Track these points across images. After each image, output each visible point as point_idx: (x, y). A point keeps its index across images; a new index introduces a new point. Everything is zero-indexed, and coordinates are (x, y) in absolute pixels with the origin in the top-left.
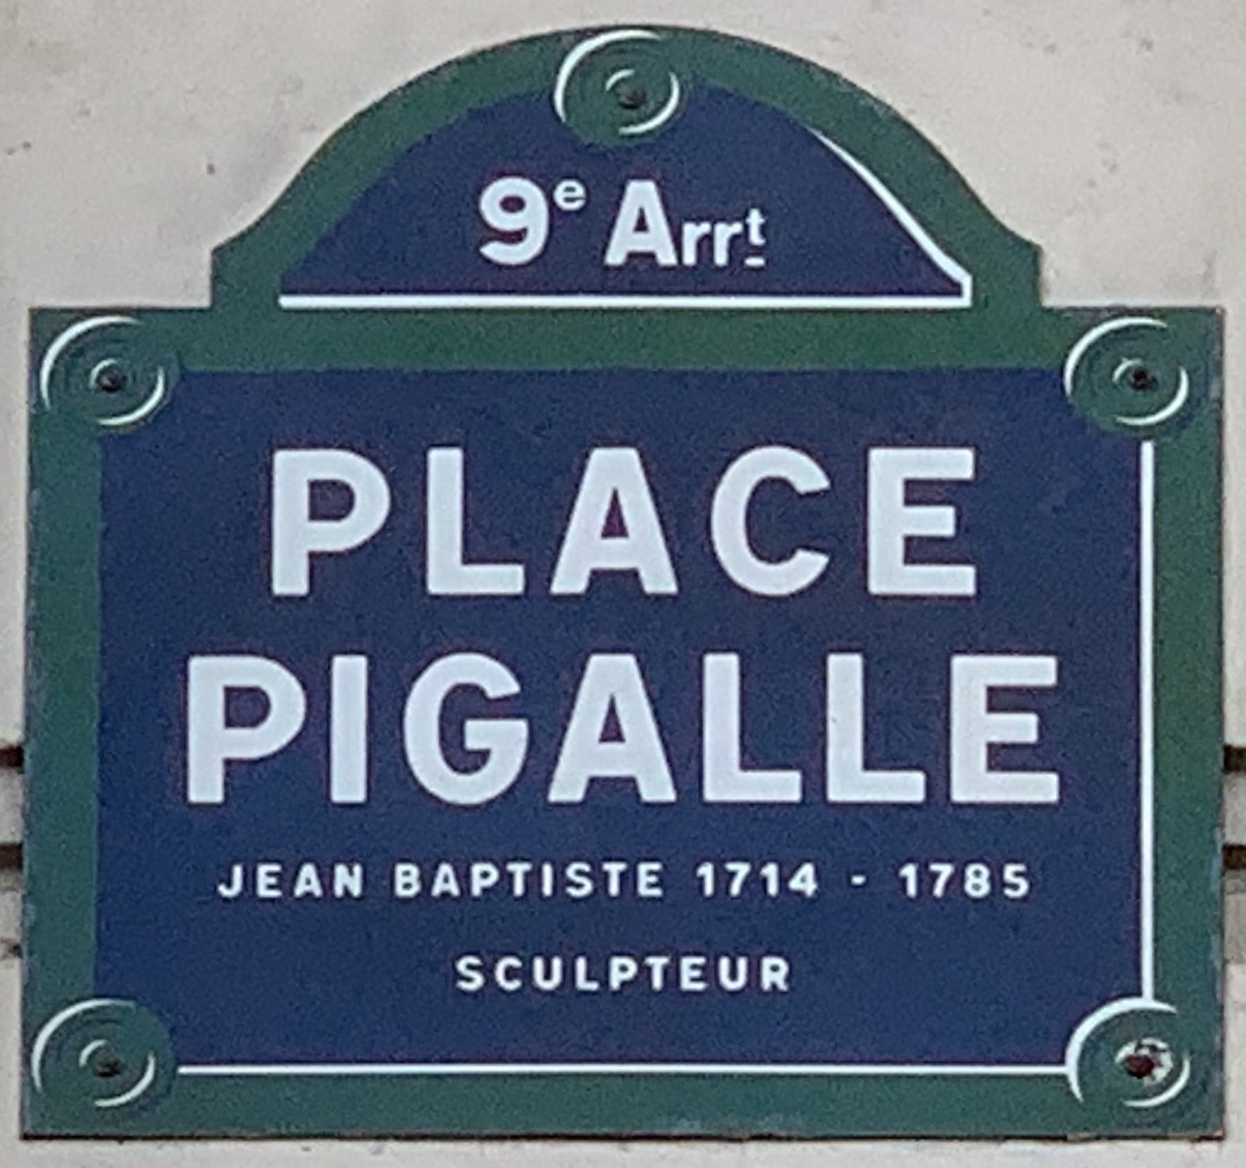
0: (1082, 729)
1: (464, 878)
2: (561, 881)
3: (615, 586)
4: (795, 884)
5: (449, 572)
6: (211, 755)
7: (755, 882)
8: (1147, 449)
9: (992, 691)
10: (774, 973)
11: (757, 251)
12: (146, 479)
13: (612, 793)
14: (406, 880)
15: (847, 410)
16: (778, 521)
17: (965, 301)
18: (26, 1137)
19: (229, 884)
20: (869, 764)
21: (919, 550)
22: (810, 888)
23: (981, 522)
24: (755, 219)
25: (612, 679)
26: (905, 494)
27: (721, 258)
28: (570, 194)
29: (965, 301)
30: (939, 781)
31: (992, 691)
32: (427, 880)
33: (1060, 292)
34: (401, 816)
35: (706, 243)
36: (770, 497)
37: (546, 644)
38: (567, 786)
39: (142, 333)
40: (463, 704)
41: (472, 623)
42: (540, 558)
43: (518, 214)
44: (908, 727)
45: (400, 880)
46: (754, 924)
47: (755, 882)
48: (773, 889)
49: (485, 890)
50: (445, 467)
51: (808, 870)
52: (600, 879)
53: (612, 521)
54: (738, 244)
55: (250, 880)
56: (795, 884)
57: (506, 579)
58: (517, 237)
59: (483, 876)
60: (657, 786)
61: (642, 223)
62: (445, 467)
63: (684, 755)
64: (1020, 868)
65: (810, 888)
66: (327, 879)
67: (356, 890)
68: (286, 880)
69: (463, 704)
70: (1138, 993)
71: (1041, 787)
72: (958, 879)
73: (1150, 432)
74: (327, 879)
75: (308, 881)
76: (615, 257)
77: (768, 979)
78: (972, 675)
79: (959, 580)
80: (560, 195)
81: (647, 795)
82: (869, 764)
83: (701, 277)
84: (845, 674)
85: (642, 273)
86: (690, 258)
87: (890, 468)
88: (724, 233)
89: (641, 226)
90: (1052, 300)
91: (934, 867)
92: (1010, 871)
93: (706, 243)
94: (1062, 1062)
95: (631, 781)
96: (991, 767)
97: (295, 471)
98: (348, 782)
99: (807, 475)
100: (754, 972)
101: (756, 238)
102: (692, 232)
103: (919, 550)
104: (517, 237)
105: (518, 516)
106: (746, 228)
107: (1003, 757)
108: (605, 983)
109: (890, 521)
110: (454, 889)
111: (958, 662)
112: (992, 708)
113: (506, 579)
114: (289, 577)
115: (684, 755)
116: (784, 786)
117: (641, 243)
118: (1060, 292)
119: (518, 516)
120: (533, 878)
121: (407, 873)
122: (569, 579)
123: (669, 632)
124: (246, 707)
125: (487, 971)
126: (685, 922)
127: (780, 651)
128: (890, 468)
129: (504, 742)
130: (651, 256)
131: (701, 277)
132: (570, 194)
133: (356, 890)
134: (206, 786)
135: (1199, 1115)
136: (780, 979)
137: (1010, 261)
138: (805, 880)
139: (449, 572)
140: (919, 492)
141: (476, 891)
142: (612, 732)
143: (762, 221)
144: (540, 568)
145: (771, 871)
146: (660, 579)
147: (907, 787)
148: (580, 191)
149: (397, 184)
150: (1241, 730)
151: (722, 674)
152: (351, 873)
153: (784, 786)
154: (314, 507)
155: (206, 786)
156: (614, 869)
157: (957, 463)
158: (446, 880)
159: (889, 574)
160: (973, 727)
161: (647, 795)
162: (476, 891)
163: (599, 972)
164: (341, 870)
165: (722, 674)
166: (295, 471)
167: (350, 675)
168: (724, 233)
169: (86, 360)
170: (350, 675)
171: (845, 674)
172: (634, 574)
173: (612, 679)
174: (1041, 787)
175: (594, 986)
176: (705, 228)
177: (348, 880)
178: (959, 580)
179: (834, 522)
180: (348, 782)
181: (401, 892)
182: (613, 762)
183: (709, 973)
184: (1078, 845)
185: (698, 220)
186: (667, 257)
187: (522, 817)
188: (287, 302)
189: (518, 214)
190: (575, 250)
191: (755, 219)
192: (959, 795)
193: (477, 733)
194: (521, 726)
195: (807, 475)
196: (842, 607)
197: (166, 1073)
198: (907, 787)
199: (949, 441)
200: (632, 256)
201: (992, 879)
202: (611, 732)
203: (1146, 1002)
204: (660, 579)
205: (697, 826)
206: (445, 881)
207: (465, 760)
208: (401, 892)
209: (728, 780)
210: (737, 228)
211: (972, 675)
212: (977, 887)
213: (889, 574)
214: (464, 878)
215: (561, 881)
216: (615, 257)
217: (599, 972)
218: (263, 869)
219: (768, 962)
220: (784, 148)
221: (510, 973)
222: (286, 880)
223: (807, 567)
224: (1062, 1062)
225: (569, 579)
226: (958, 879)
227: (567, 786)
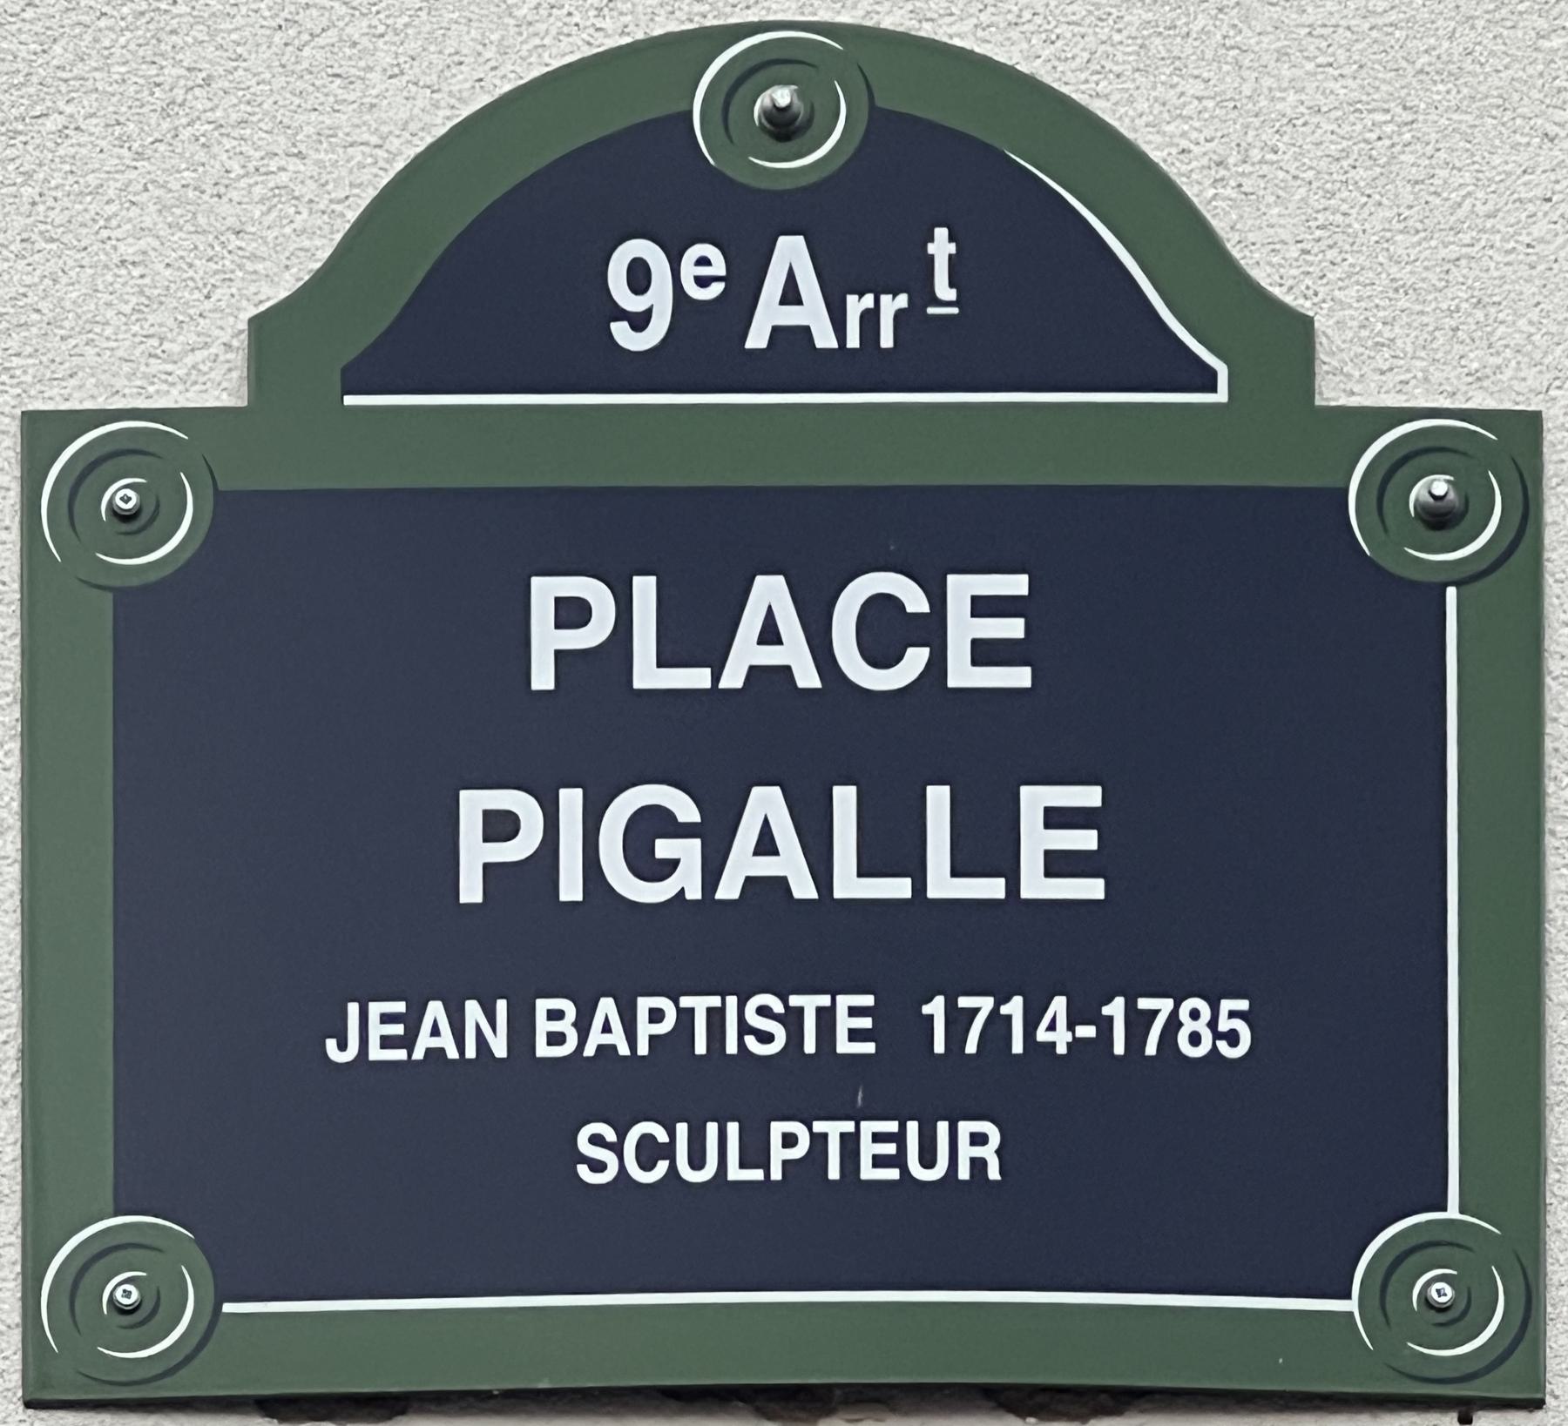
7: (998, 1025)
8: (1451, 592)
17: (1221, 396)
29: (1221, 396)
33: (1342, 383)
35: (870, 319)
39: (150, 445)
40: (651, 823)
43: (651, 286)
47: (998, 1025)
56: (1042, 1035)
58: (640, 322)
61: (793, 294)
63: (822, 870)
73: (1465, 577)
85: (793, 358)
86: (853, 341)
87: (962, 588)
88: (892, 304)
90: (1331, 392)
93: (870, 319)
98: (571, 888)
102: (855, 306)
109: (963, 629)
115: (822, 870)
118: (1342, 383)
143: (952, 248)
148: (719, 267)
149: (498, 245)
160: (1035, 840)
167: (571, 800)
170: (571, 800)
176: (868, 301)
180: (571, 888)
186: (825, 338)
188: (349, 400)
189: (651, 286)
193: (664, 848)
194: (697, 842)
207: (650, 869)
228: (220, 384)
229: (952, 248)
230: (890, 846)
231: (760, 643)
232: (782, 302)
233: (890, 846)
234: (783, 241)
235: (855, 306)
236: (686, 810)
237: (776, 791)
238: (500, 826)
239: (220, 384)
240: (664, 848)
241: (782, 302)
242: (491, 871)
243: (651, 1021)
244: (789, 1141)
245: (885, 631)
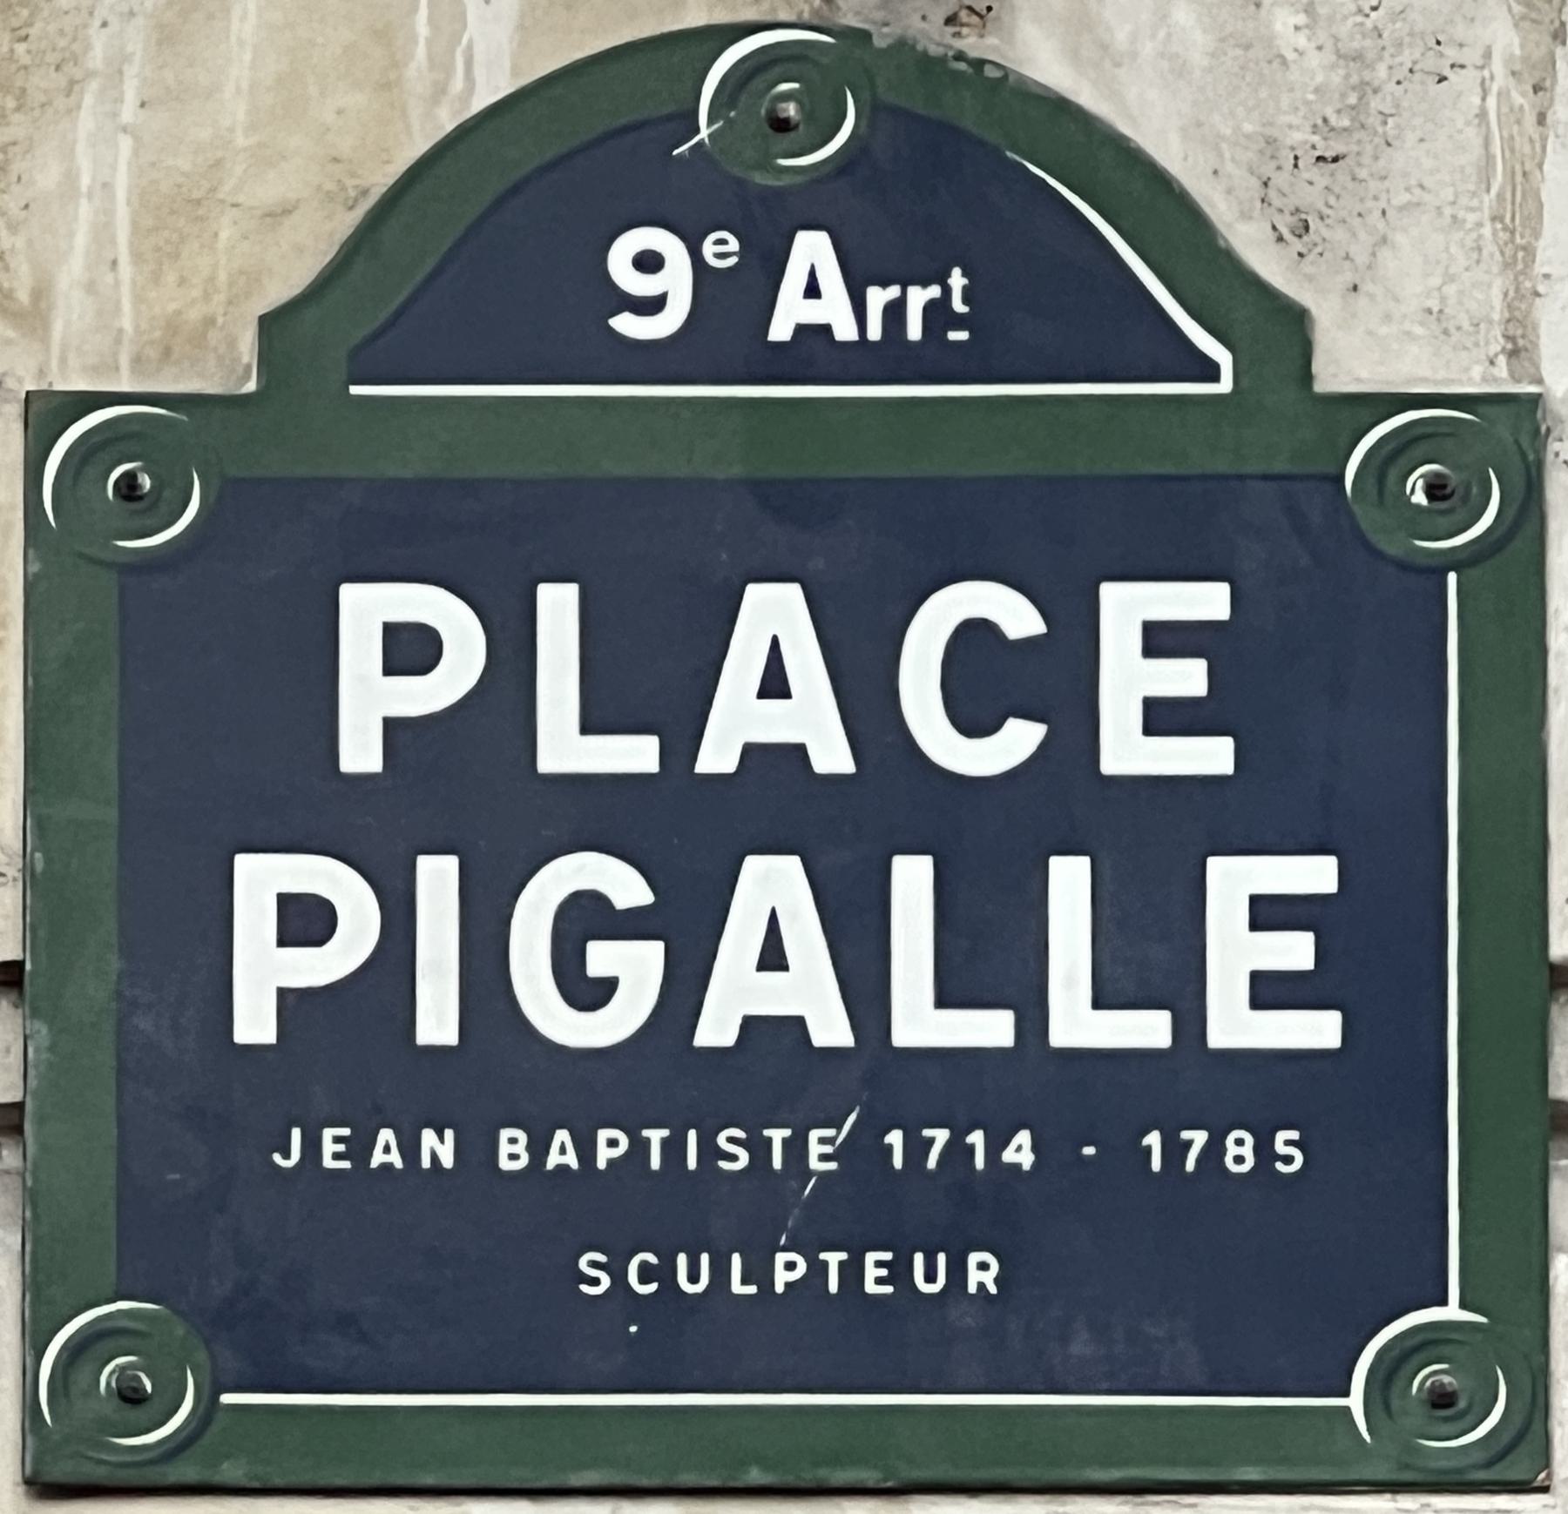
1: (586, 1149)
2: (710, 1152)
3: (776, 763)
4: (1009, 1156)
5: (564, 746)
6: (263, 979)
7: (958, 1151)
8: (1452, 578)
9: (1257, 978)
10: (982, 1272)
11: (959, 322)
12: (183, 594)
13: (773, 1036)
14: (512, 1150)
16: (982, 679)
17: (1225, 385)
19: (286, 1155)
21: (1162, 717)
22: (1026, 1159)
23: (1242, 681)
24: (957, 280)
25: (772, 887)
26: (1143, 641)
27: (914, 331)
29: (1225, 385)
31: (1257, 978)
32: (539, 1148)
33: (1342, 366)
34: (502, 1065)
35: (895, 312)
37: (689, 839)
38: (716, 1028)
39: (170, 433)
40: (584, 918)
42: (682, 731)
44: (1152, 953)
45: (504, 1149)
47: (958, 1151)
48: (980, 1162)
49: (611, 1162)
50: (558, 608)
51: (1024, 1138)
52: (759, 1148)
53: (774, 685)
54: (937, 313)
55: (312, 1146)
56: (1009, 1156)
57: (638, 754)
58: (653, 306)
59: (610, 1146)
60: (831, 1028)
61: (814, 289)
62: (558, 608)
63: (865, 986)
64: (1294, 1135)
65: (1026, 1159)
66: (410, 1149)
67: (447, 1161)
68: (358, 1148)
69: (584, 918)
70: (1443, 1301)
71: (1319, 1030)
72: (1215, 1149)
73: (1461, 561)
74: (410, 1149)
76: (780, 330)
77: (974, 1278)
78: (1232, 881)
79: (1212, 756)
80: (708, 249)
81: (820, 1039)
83: (886, 357)
84: (1070, 881)
86: (875, 332)
87: (1125, 607)
88: (918, 298)
89: (812, 291)
91: (1186, 1135)
92: (1283, 1140)
93: (895, 312)
94: (1346, 1394)
95: (800, 1022)
96: (1255, 926)
98: (437, 1020)
99: (1018, 617)
100: (958, 1271)
101: (959, 306)
102: (877, 298)
104: (653, 306)
105: (650, 676)
106: (947, 291)
108: (766, 1282)
109: (1127, 678)
110: (571, 1160)
111: (1215, 865)
112: (1257, 1003)
113: (638, 754)
114: (360, 752)
115: (865, 986)
116: (992, 1029)
117: (813, 313)
118: (1342, 366)
119: (650, 676)
120: (674, 1148)
121: (513, 1141)
122: (717, 755)
123: (846, 825)
124: (305, 921)
125: (618, 1274)
126: (867, 1205)
127: (990, 851)
128: (1125, 607)
129: (635, 968)
130: (826, 329)
132: (721, 249)
133: (447, 1161)
134: (255, 1022)
135: (1520, 1459)
136: (988, 1278)
138: (1020, 1152)
139: (564, 746)
140: (1161, 640)
141: (601, 1164)
142: (773, 957)
143: (965, 281)
144: (682, 738)
145: (977, 1138)
146: (832, 755)
147: (1149, 1029)
148: (734, 245)
150: (1566, 944)
151: (912, 880)
152: (434, 1157)
153: (992, 1029)
154: (391, 660)
155: (255, 1022)
156: (778, 1136)
157: (1209, 601)
158: (563, 1151)
159: (1126, 750)
160: (1234, 951)
161: (820, 1039)
162: (601, 1164)
163: (759, 1272)
164: (428, 1137)
165: (912, 880)
167: (437, 879)
168: (918, 298)
169: (103, 456)
170: (437, 879)
171: (1070, 881)
172: (800, 751)
173: (772, 887)
174: (1319, 1030)
175: (752, 1289)
176: (894, 292)
177: (439, 1147)
178: (1212, 756)
179: (1054, 677)
180: (437, 1020)
181: (505, 1164)
182: (774, 997)
183: (898, 1273)
184: (1367, 1102)
185: (884, 284)
186: (845, 330)
188: (355, 390)
189: (657, 275)
190: (730, 317)
191: (957, 280)
192: (1218, 1038)
193: (601, 957)
195: (1018, 617)
196: (1066, 796)
198: (1149, 1029)
200: (801, 330)
201: (1257, 1150)
202: (772, 960)
203: (1451, 1312)
204: (832, 755)
205: (882, 1076)
206: (562, 1153)
207: (590, 994)
208: (505, 1164)
209: (920, 1021)
210: (934, 291)
211: (1232, 881)
212: (1239, 1160)
213: (1126, 750)
214: (586, 1149)
215: (710, 1152)
217: (759, 1272)
218: (328, 1134)
219: (974, 1258)
220: (991, 191)
221: (646, 1274)
222: (358, 1148)
223: (1018, 740)
224: (1346, 1394)
225: (717, 755)
226: (1215, 1149)
227: (716, 1028)
229: (965, 281)
230: (990, 953)
231: (785, 968)
232: (762, 694)
233: (990, 953)
234: (754, 865)
235: (877, 298)
236: (626, 887)
237: (791, 865)
238: (305, 921)
240: (601, 957)
241: (762, 694)
242: (290, 1001)
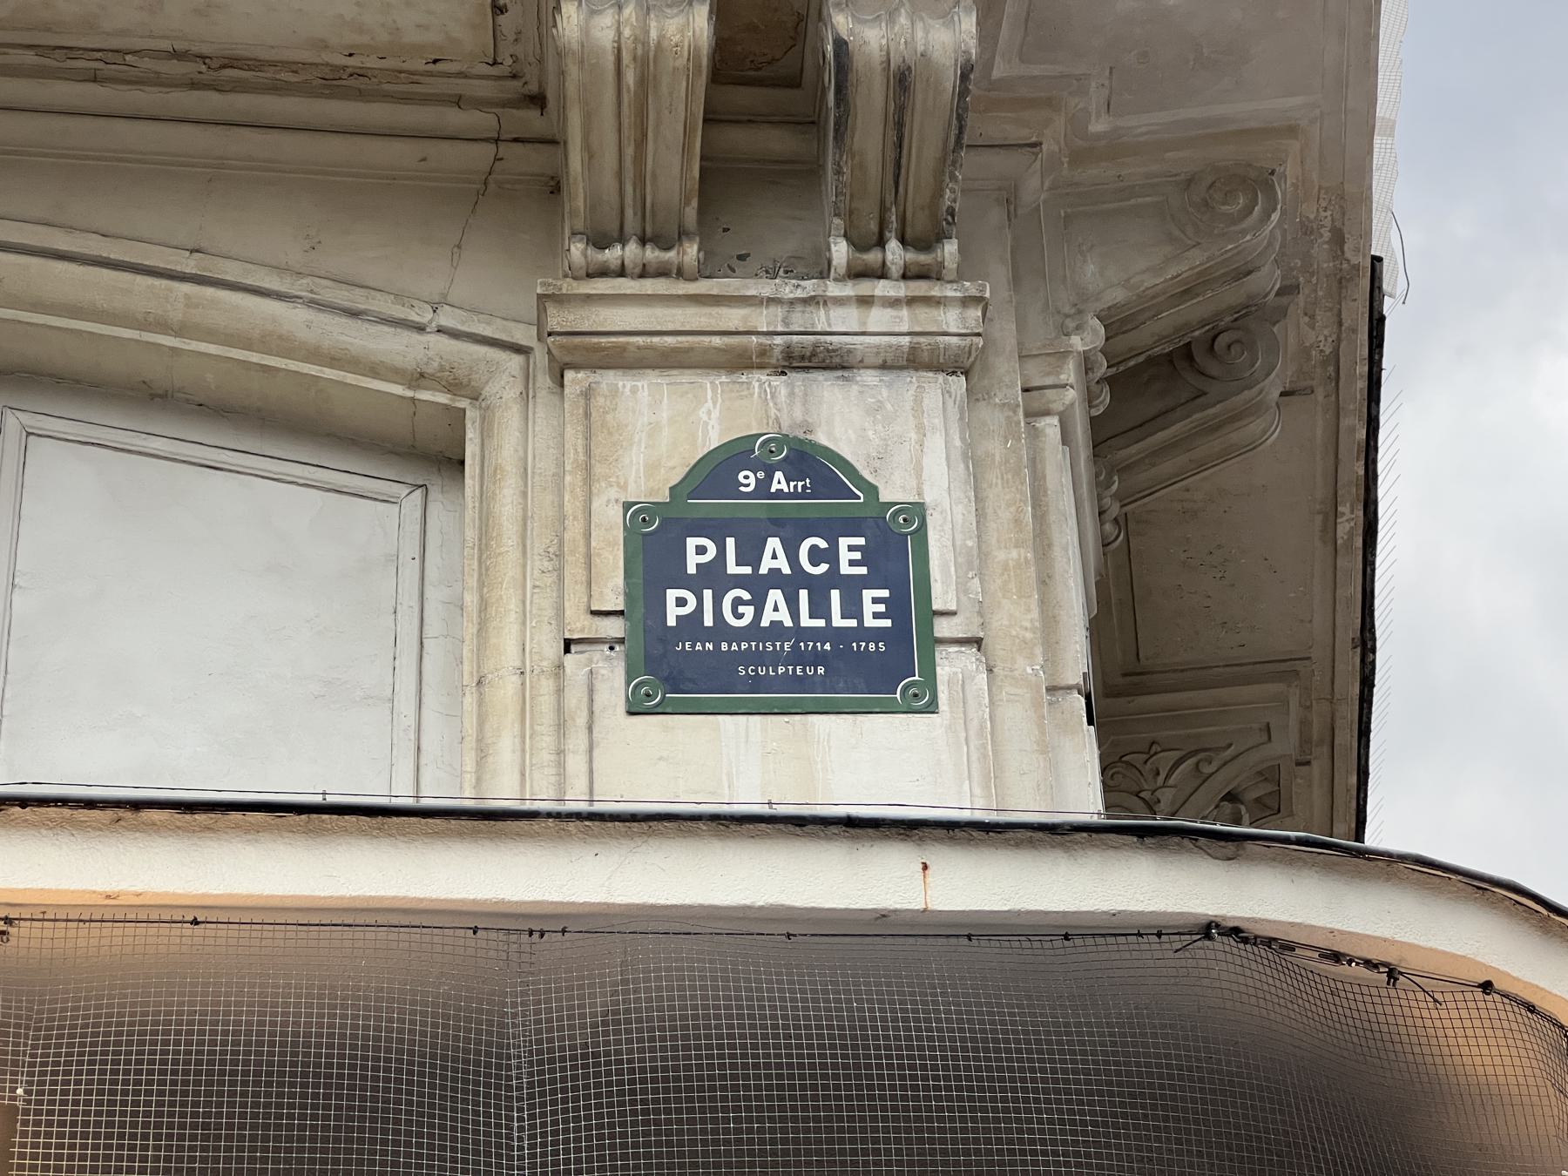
0: (896, 607)
3: (775, 572)
5: (732, 568)
6: (673, 614)
7: (815, 647)
13: (776, 625)
14: (724, 647)
15: (833, 528)
16: (816, 556)
18: (631, 713)
20: (843, 617)
21: (852, 563)
25: (775, 595)
26: (848, 549)
28: (761, 475)
30: (861, 622)
33: (885, 497)
34: (721, 630)
36: (814, 549)
37: (758, 587)
38: (765, 623)
40: (738, 602)
41: (739, 582)
42: (756, 565)
44: (852, 607)
46: (817, 658)
47: (815, 647)
50: (730, 542)
53: (774, 556)
57: (747, 570)
59: (744, 646)
60: (788, 623)
61: (779, 482)
62: (730, 542)
63: (795, 614)
68: (693, 646)
69: (738, 602)
71: (887, 623)
73: (910, 533)
75: (699, 647)
76: (773, 490)
78: (868, 595)
79: (863, 570)
82: (843, 617)
83: (794, 495)
84: (835, 595)
85: (779, 494)
87: (844, 542)
97: (692, 543)
98: (708, 621)
99: (823, 544)
103: (852, 563)
105: (751, 554)
107: (876, 616)
109: (845, 556)
113: (747, 570)
114: (692, 570)
115: (795, 614)
118: (885, 497)
122: (763, 570)
123: (790, 584)
127: (819, 590)
128: (844, 542)
129: (748, 612)
131: (794, 495)
134: (671, 622)
137: (872, 490)
138: (827, 647)
139: (732, 568)
140: (875, 601)
142: (776, 609)
144: (756, 567)
146: (786, 570)
151: (804, 595)
153: (821, 623)
154: (697, 552)
155: (671, 622)
159: (845, 569)
160: (869, 608)
165: (804, 595)
166: (692, 543)
167: (708, 594)
170: (708, 594)
171: (835, 595)
173: (775, 595)
174: (887, 623)
177: (709, 646)
178: (863, 570)
179: (831, 556)
180: (708, 621)
183: (804, 670)
184: (898, 637)
187: (754, 629)
189: (748, 480)
190: (763, 489)
193: (741, 609)
195: (823, 544)
196: (834, 578)
197: (663, 698)
198: (853, 623)
199: (707, 164)
202: (776, 609)
204: (786, 570)
205: (799, 632)
206: (734, 647)
207: (739, 616)
209: (806, 621)
211: (868, 595)
213: (845, 569)
216: (773, 490)
222: (693, 646)
223: (824, 568)
225: (763, 570)
227: (765, 623)
228: (664, 497)
230: (820, 608)
233: (820, 608)
236: (746, 596)
239: (664, 497)
240: (741, 609)
243: (677, 599)
244: (681, 602)
245: (816, 556)
